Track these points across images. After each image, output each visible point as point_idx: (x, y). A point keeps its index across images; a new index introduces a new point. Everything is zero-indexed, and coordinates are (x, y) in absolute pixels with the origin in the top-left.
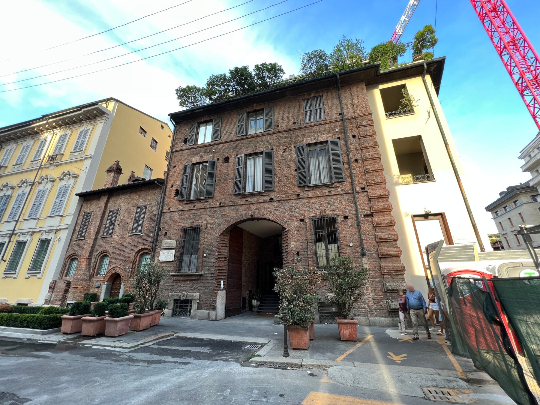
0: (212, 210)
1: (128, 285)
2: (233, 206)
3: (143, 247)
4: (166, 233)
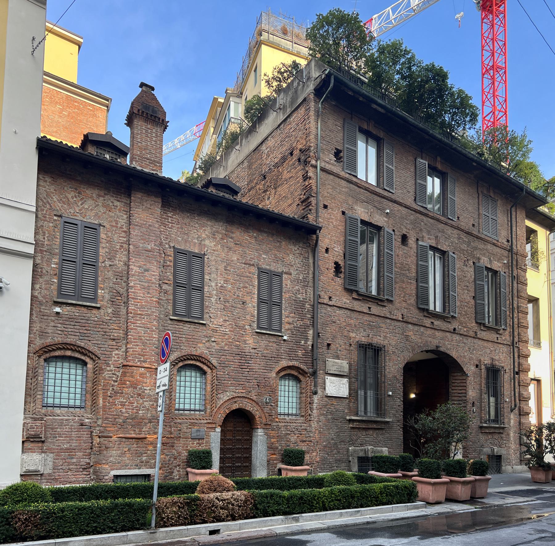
1: (273, 433)
2: (417, 325)
3: (291, 364)
4: (329, 345)
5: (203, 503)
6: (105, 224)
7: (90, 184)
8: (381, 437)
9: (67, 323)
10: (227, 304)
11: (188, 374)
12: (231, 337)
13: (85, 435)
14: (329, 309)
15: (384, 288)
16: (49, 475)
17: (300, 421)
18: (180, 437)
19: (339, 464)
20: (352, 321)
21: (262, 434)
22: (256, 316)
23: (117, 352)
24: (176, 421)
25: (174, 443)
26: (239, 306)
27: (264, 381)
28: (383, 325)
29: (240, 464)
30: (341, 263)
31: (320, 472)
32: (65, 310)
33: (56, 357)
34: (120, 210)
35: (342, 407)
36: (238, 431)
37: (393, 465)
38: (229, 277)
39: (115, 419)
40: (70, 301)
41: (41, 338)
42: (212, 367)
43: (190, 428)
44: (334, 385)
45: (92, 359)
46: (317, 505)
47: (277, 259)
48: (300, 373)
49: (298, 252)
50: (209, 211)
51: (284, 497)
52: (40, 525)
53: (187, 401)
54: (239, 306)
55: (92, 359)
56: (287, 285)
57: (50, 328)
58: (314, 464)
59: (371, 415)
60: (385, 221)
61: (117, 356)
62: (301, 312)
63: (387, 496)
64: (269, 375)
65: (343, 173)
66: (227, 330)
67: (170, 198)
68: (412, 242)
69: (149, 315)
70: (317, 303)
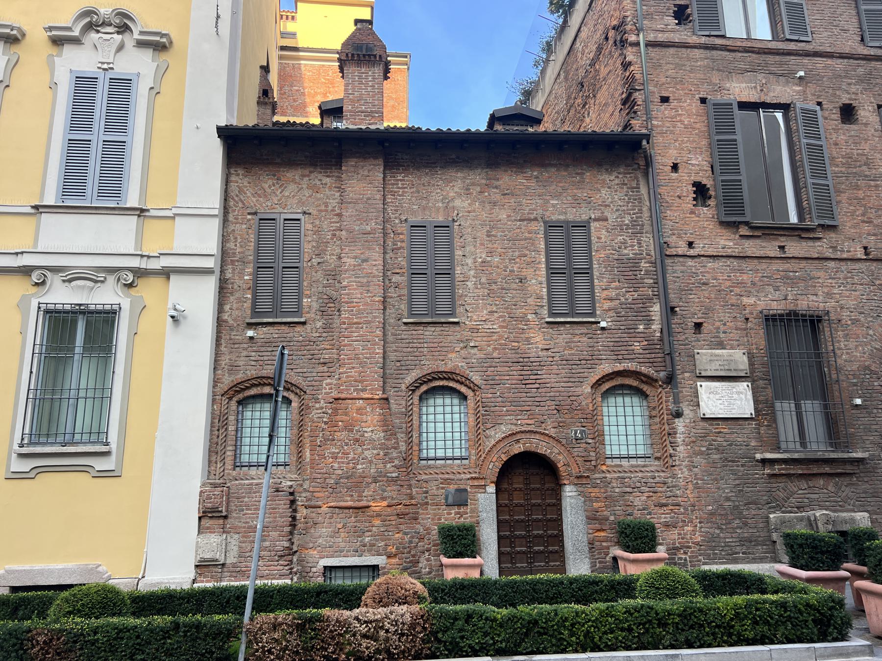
0: (844, 266)
3: (619, 367)
4: (698, 326)
5: (328, 626)
6: (310, 211)
7: (292, 164)
8: (847, 491)
9: (263, 349)
10: (494, 287)
11: (439, 401)
12: (503, 336)
13: (283, 505)
14: (690, 262)
15: (810, 208)
16: (234, 565)
17: (652, 469)
18: (427, 503)
19: (748, 548)
20: (745, 277)
21: (574, 494)
22: (545, 297)
23: (329, 381)
24: (419, 477)
25: (418, 513)
26: (514, 286)
27: (568, 402)
28: (821, 274)
29: (542, 548)
30: (708, 182)
31: (705, 564)
32: (261, 333)
33: (254, 397)
34: (330, 188)
35: (743, 436)
36: (533, 489)
37: (823, 553)
38: (495, 246)
39: (325, 479)
40: (265, 320)
41: (230, 374)
42: (474, 388)
43: (443, 488)
44: (717, 397)
45: (297, 394)
46: (574, 639)
47: (577, 202)
48: (643, 382)
49: (617, 181)
50: (458, 158)
51: (495, 620)
52: (65, 652)
53: (440, 444)
54: (514, 286)
55: (297, 394)
56: (599, 238)
57: (242, 358)
58: (690, 547)
59: (818, 446)
60: (798, 92)
61: (328, 388)
62: (633, 277)
63: (756, 623)
64: (578, 390)
65: (694, 38)
66: (495, 327)
67: (399, 154)
68: (867, 114)
69: (368, 322)
70: (664, 254)
